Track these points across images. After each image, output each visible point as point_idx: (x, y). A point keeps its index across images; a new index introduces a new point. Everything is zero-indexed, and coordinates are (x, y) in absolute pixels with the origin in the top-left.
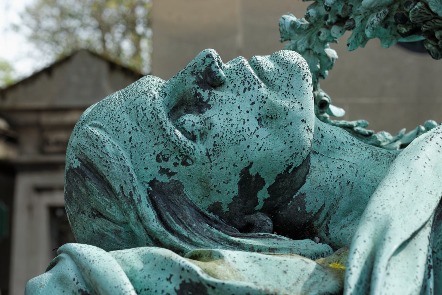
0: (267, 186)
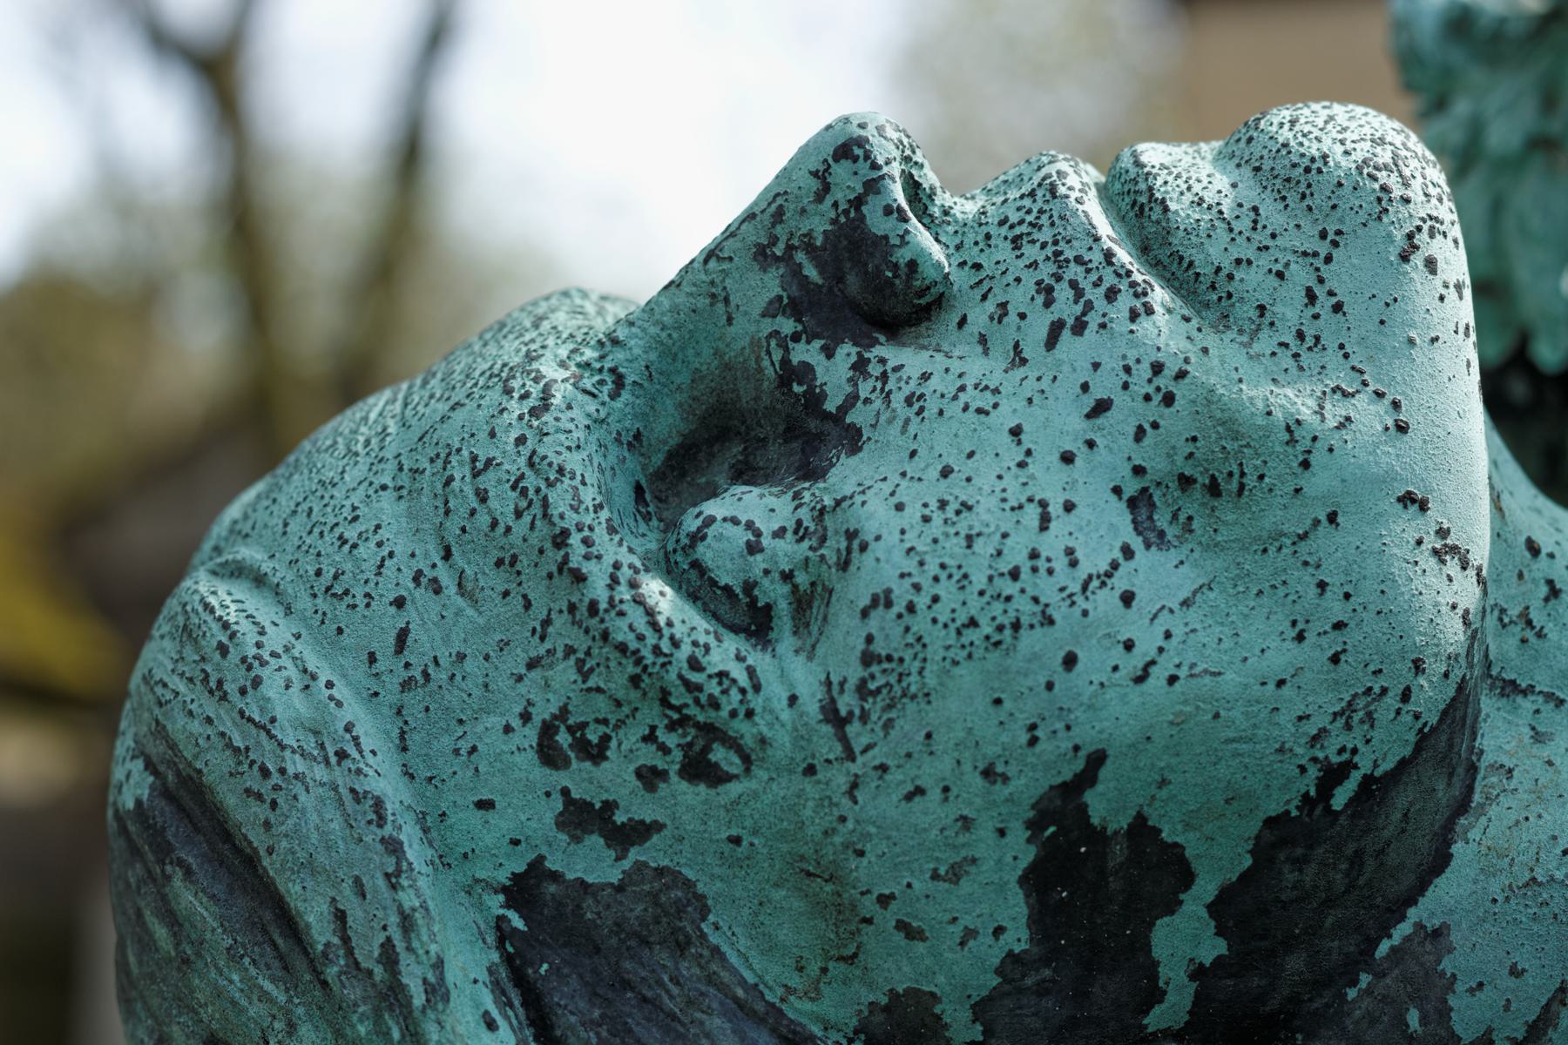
0: (1206, 888)
